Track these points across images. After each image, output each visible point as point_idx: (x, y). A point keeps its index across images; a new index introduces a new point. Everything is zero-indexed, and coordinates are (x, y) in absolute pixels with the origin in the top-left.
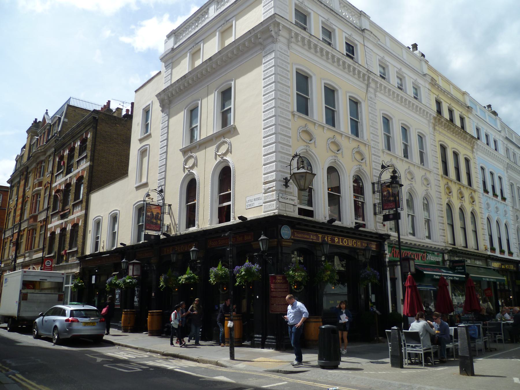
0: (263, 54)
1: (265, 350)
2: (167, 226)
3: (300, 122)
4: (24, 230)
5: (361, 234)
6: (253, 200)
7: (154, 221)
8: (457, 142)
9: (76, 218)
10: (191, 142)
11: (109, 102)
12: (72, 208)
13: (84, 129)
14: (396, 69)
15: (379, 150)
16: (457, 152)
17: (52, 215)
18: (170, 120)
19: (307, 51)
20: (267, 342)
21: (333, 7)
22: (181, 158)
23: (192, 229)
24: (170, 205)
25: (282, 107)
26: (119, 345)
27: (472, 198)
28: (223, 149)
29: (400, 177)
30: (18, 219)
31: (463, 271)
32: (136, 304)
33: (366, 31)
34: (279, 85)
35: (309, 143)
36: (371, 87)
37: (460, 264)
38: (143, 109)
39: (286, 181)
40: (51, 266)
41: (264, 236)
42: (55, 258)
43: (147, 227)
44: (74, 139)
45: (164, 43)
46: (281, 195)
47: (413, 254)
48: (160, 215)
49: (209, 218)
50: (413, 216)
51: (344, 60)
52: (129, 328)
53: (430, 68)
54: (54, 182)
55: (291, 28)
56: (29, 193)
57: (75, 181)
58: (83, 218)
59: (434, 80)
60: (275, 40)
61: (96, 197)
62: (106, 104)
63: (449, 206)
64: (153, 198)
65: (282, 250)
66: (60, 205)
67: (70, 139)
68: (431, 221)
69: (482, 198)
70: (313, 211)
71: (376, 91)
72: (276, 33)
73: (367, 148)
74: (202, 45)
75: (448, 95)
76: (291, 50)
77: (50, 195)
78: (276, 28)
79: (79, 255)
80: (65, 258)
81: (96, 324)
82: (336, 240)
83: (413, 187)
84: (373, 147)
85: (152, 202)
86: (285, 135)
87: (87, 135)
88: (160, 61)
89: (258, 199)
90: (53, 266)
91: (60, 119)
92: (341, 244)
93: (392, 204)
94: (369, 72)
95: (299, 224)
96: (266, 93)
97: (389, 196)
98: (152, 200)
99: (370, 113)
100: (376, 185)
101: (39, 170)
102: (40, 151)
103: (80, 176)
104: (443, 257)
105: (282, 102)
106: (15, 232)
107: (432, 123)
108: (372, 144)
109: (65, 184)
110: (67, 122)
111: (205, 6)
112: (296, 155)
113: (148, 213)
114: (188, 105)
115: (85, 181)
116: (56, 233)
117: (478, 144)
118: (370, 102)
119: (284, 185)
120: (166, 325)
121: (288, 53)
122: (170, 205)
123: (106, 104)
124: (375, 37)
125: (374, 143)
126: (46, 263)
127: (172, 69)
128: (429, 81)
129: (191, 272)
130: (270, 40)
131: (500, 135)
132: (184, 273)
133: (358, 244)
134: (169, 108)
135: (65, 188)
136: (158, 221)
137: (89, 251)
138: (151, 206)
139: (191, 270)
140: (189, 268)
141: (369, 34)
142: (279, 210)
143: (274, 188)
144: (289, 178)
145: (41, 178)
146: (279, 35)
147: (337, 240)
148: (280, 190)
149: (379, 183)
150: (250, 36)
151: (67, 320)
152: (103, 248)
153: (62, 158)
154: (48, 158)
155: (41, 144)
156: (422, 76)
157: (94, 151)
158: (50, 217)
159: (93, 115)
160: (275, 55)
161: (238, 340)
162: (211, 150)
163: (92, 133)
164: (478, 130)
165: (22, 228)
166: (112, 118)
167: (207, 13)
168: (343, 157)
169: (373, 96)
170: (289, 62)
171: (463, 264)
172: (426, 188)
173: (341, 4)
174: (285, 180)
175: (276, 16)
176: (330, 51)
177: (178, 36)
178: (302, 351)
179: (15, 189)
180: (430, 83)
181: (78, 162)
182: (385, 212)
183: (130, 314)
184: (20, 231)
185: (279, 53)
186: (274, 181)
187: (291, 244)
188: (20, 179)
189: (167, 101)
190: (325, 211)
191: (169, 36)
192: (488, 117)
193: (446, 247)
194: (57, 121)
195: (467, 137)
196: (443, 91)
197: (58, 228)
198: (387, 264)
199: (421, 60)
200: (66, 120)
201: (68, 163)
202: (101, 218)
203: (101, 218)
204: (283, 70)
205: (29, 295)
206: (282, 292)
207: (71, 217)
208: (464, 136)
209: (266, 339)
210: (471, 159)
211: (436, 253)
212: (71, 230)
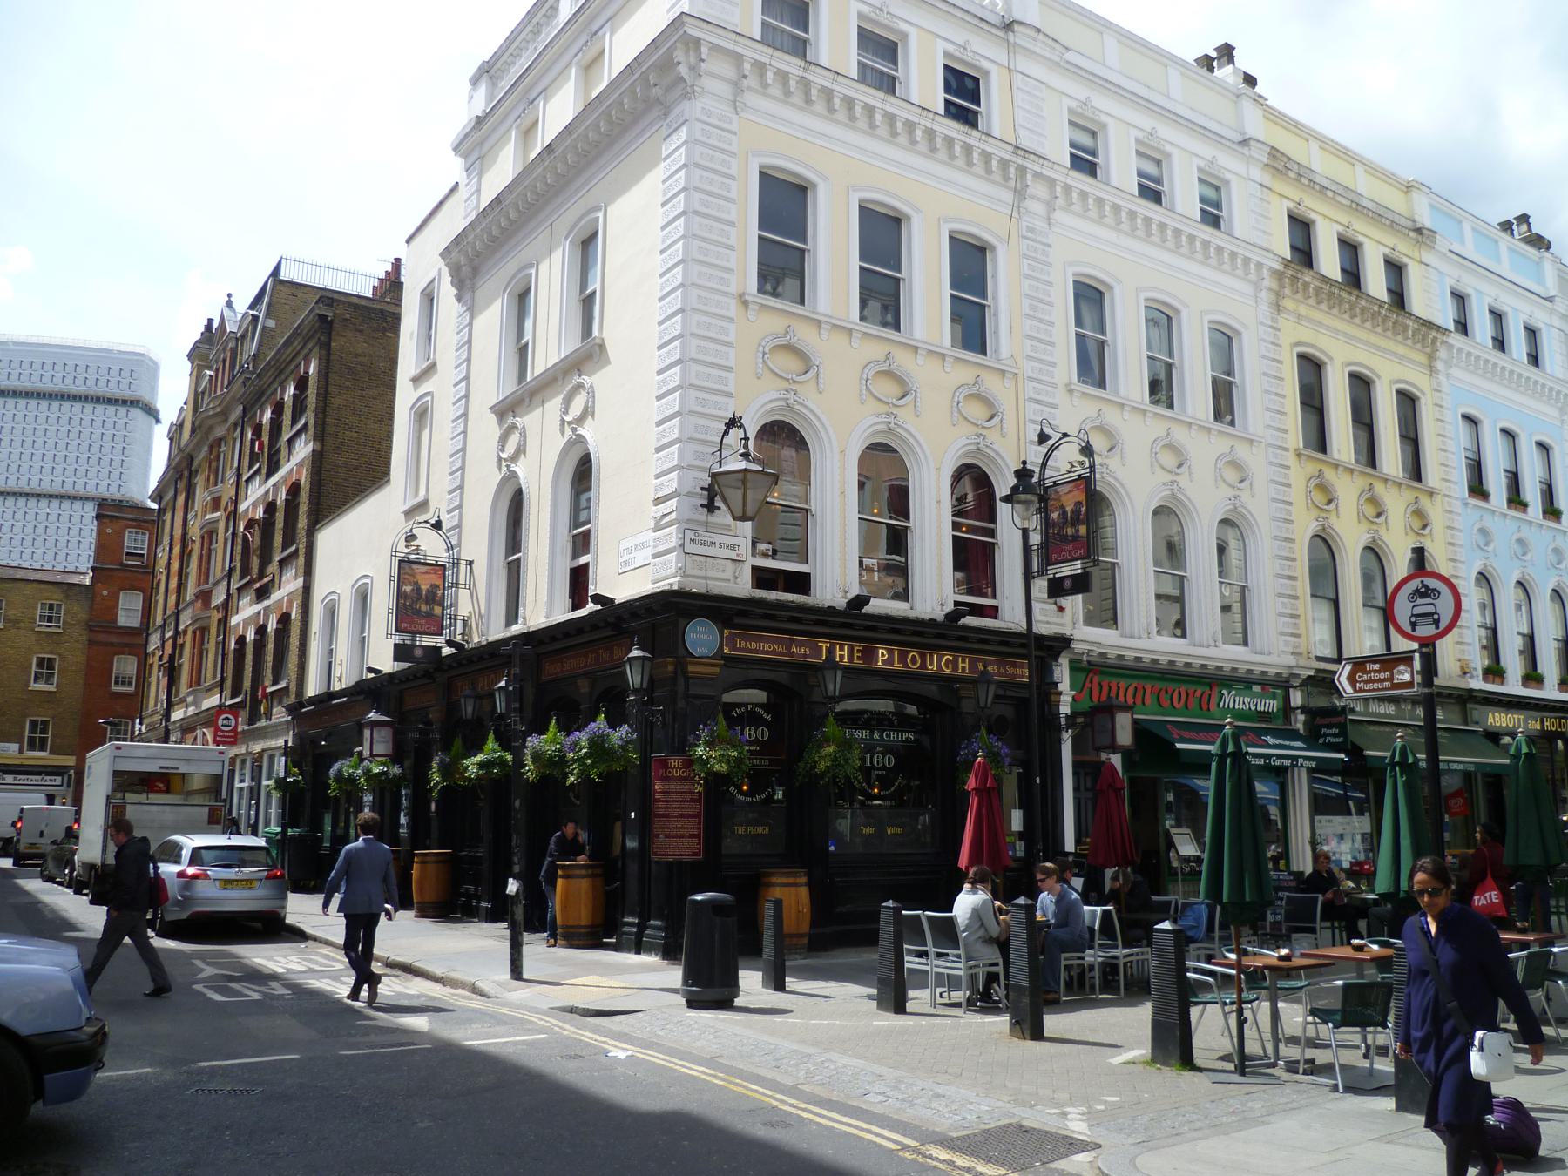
0: (664, 132)
1: (644, 959)
3: (771, 318)
4: (185, 631)
7: (424, 607)
8: (1366, 343)
10: (520, 383)
13: (302, 348)
15: (1054, 385)
16: (1360, 373)
17: (238, 589)
18: (475, 322)
23: (517, 629)
24: (471, 563)
26: (315, 939)
27: (1419, 513)
30: (172, 599)
31: (1341, 740)
33: (1016, 27)
36: (1033, 197)
37: (1334, 720)
38: (422, 293)
40: (235, 730)
42: (245, 707)
43: (404, 625)
44: (283, 377)
46: (690, 534)
47: (1167, 692)
48: (440, 592)
51: (929, 125)
53: (1277, 118)
54: (243, 498)
55: (739, 50)
56: (195, 532)
58: (300, 598)
59: (1279, 155)
65: (687, 688)
66: (255, 562)
67: (275, 379)
68: (1249, 590)
69: (1459, 515)
70: (809, 574)
71: (1051, 207)
72: (692, 68)
73: (1010, 383)
75: (1339, 198)
76: (742, 114)
77: (234, 534)
78: (691, 53)
79: (292, 699)
83: (1181, 490)
84: (1031, 379)
87: (307, 367)
89: (643, 545)
90: (239, 729)
92: (897, 666)
96: (666, 244)
99: (1027, 276)
101: (214, 464)
102: (211, 413)
104: (1287, 699)
105: (704, 269)
106: (167, 636)
107: (1270, 289)
108: (1028, 368)
113: (404, 587)
114: (511, 279)
116: (248, 640)
117: (1451, 346)
119: (702, 505)
120: (463, 890)
121: (731, 123)
122: (471, 563)
123: (390, 269)
124: (1050, 42)
125: (1036, 365)
126: (220, 722)
127: (480, 175)
128: (1262, 162)
129: (497, 746)
130: (678, 92)
131: (1552, 311)
132: (477, 747)
133: (961, 665)
137: (313, 689)
138: (415, 566)
140: (491, 736)
141: (1029, 37)
142: (684, 575)
143: (674, 516)
145: (220, 485)
146: (700, 75)
147: (883, 655)
150: (632, 80)
151: (181, 875)
154: (232, 430)
155: (219, 392)
157: (324, 412)
158: (236, 596)
159: (318, 311)
161: (589, 930)
162: (554, 404)
163: (317, 361)
164: (1460, 299)
165: (181, 628)
169: (1040, 224)
171: (1341, 719)
172: (1231, 492)
174: (706, 493)
175: (685, 19)
179: (168, 516)
180: (1267, 165)
181: (291, 441)
182: (1054, 571)
184: (177, 633)
187: (717, 670)
188: (176, 488)
190: (846, 575)
191: (475, 81)
192: (1509, 255)
193: (1290, 667)
195: (1406, 328)
196: (1317, 187)
199: (1238, 96)
200: (271, 323)
202: (336, 598)
205: (129, 808)
208: (1394, 323)
209: (646, 929)
210: (1424, 394)
211: (1257, 689)
212: (277, 629)
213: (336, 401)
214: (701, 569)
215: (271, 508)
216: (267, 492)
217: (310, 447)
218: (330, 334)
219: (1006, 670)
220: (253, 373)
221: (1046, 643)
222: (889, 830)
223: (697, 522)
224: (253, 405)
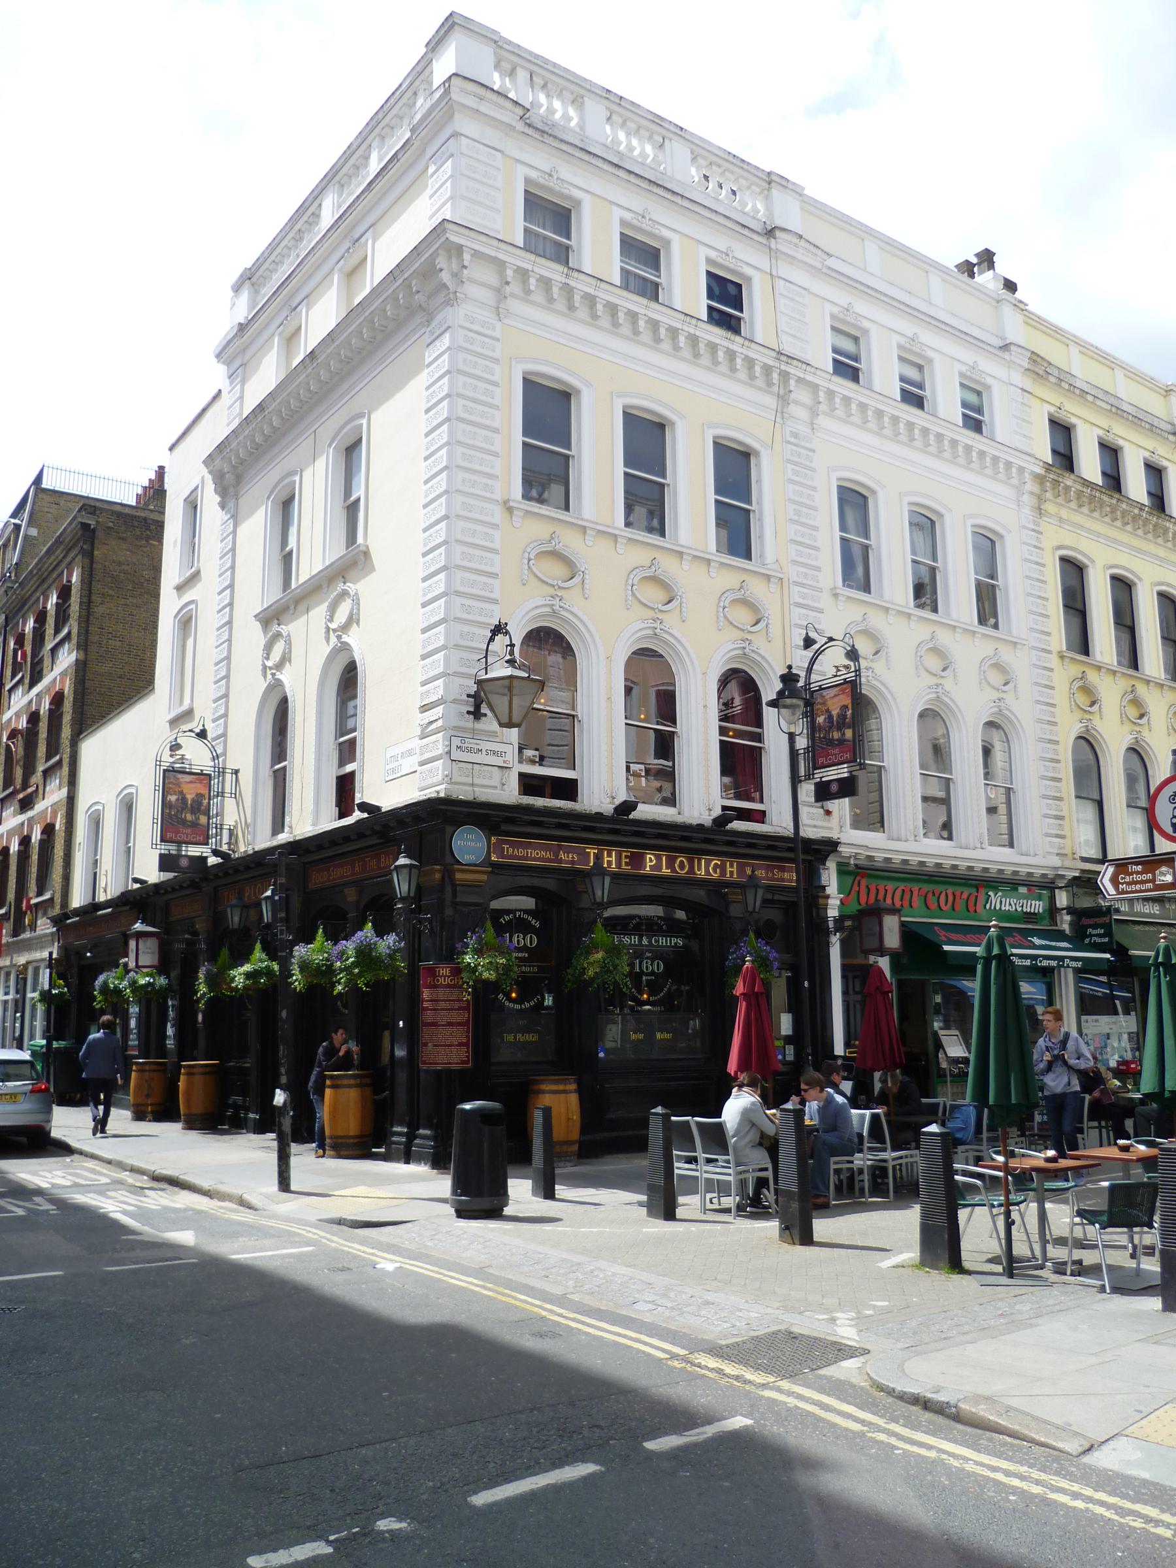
2: (230, 829)
5: (734, 841)
7: (189, 817)
13: (65, 557)
14: (896, 339)
15: (820, 590)
19: (566, 315)
20: (418, 1146)
21: (669, 173)
23: (283, 838)
24: (236, 772)
25: (471, 490)
31: (1106, 940)
32: (170, 1043)
34: (461, 426)
35: (560, 588)
36: (796, 403)
38: (185, 500)
41: (404, 857)
42: (9, 919)
44: (45, 586)
46: (456, 742)
48: (205, 802)
49: (312, 807)
50: (949, 779)
51: (692, 331)
52: (150, 1108)
55: (501, 256)
59: (1039, 360)
60: (451, 296)
61: (93, 748)
62: (153, 477)
63: (1087, 743)
71: (814, 413)
72: (455, 275)
74: (304, 311)
75: (1099, 403)
76: (506, 321)
79: (57, 911)
80: (29, 920)
81: (21, 1098)
83: (947, 693)
84: (797, 583)
86: (476, 570)
87: (70, 575)
88: (216, 360)
89: (410, 753)
92: (666, 871)
94: (784, 358)
95: (511, 821)
104: (1052, 899)
107: (1032, 493)
108: (793, 573)
110: (34, 538)
111: (311, 199)
118: (790, 447)
119: (468, 712)
120: (230, 1102)
122: (236, 772)
123: (153, 477)
124: (812, 248)
127: (243, 382)
128: (1021, 366)
129: (264, 956)
130: (440, 298)
133: (729, 869)
135: (30, 726)
136: (201, 817)
138: (180, 776)
139: (264, 949)
140: (258, 946)
143: (440, 723)
147: (651, 860)
148: (455, 728)
150: (395, 286)
152: (105, 891)
153: (20, 640)
156: (996, 351)
157: (87, 621)
159: (80, 520)
160: (452, 339)
161: (358, 1140)
162: (319, 612)
163: (80, 570)
166: (136, 524)
167: (316, 216)
169: (803, 429)
170: (497, 355)
171: (1107, 920)
174: (472, 700)
175: (447, 225)
176: (641, 310)
177: (259, 286)
178: (510, 1171)
181: (54, 650)
182: (821, 775)
183: (150, 1071)
185: (462, 332)
186: (441, 701)
187: (484, 877)
189: (229, 478)
191: (237, 288)
193: (1056, 868)
195: (1166, 530)
196: (1077, 392)
197: (14, 836)
199: (998, 302)
200: (33, 532)
201: (33, 658)
203: (101, 808)
204: (475, 382)
206: (449, 1010)
207: (40, 806)
213: (99, 610)
215: (34, 718)
216: (31, 702)
219: (774, 874)
222: (659, 1036)
223: (463, 729)
224: (16, 613)
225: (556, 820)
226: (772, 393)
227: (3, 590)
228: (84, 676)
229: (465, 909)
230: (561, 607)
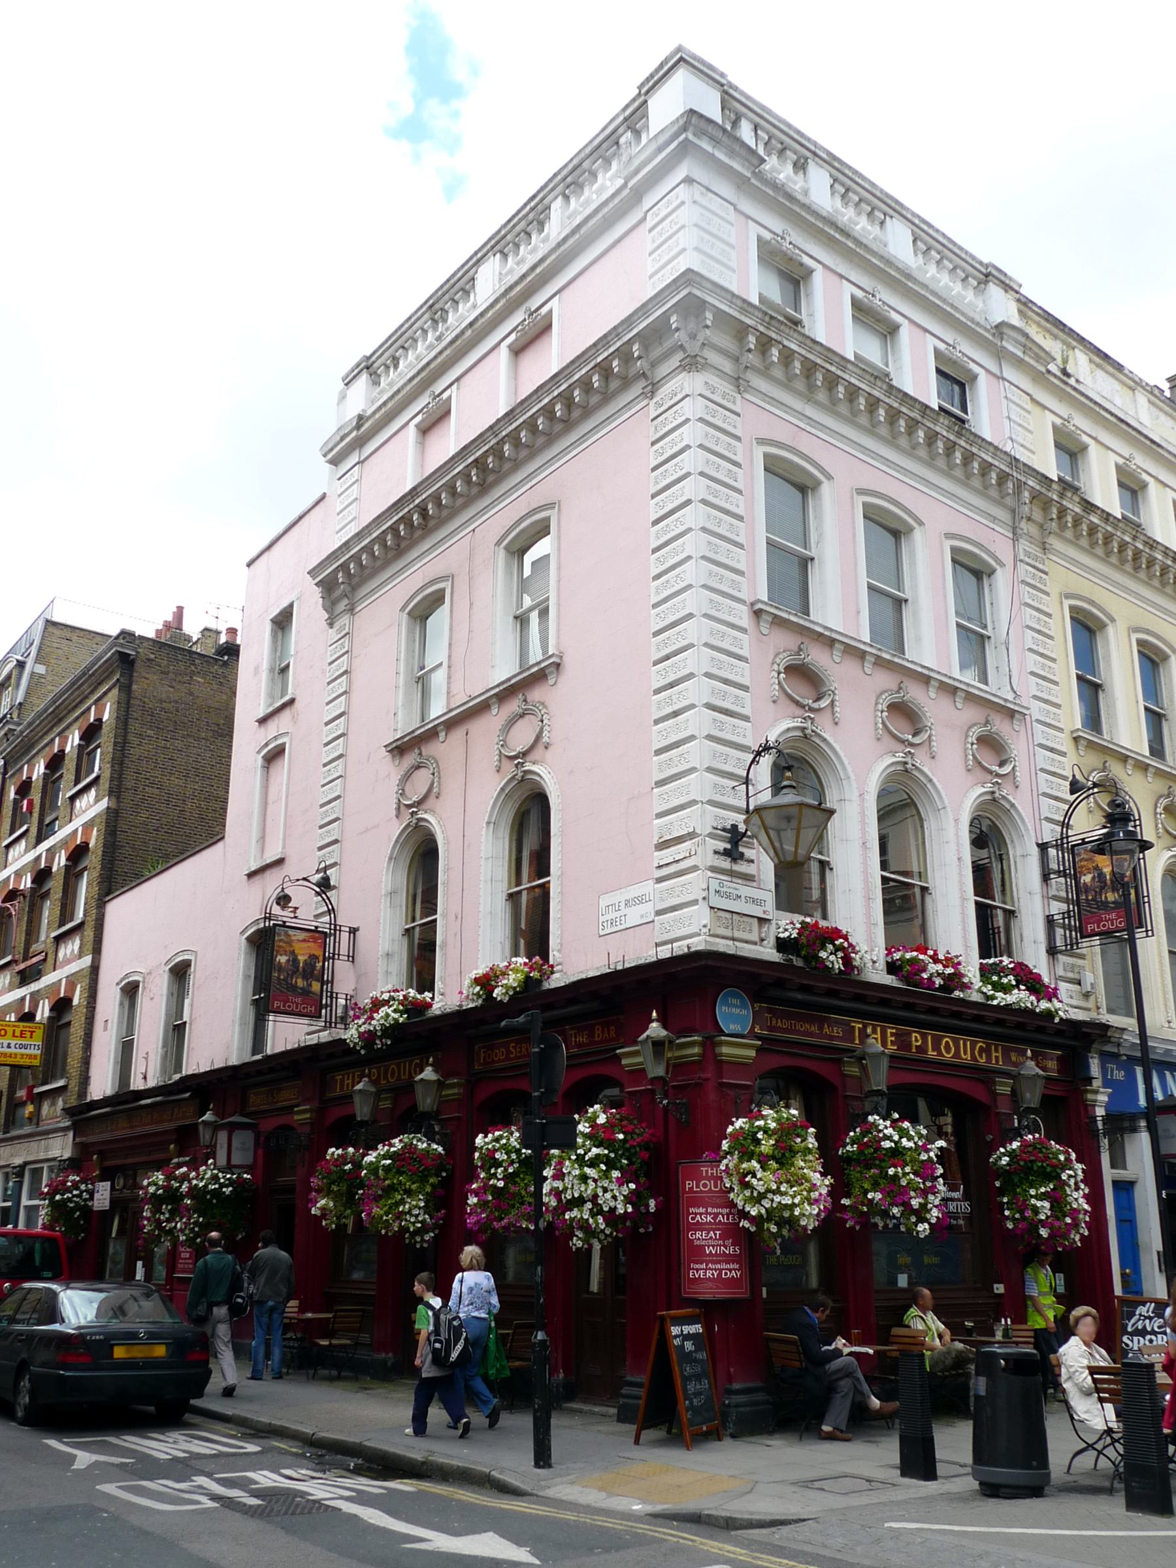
6: (622, 904)
7: (300, 983)
9: (64, 980)
11: (180, 609)
12: (53, 949)
22: (389, 771)
24: (353, 931)
28: (522, 736)
29: (1140, 819)
35: (811, 710)
39: (735, 837)
45: (336, 401)
57: (63, 862)
61: (120, 910)
64: (296, 908)
79: (73, 1101)
82: (916, 1039)
85: (294, 920)
89: (640, 900)
91: (21, 665)
92: (931, 1053)
93: (1113, 916)
97: (1102, 888)
98: (294, 912)
100: (1052, 852)
103: (78, 846)
109: (35, 873)
110: (41, 676)
112: (766, 748)
115: (93, 860)
121: (734, 403)
122: (353, 931)
133: (994, 1054)
134: (351, 610)
136: (314, 983)
137: (102, 1085)
138: (291, 932)
144: (742, 828)
147: (917, 1040)
149: (1062, 844)
152: (145, 1078)
166: (180, 657)
168: (933, 758)
173: (919, 243)
194: (11, 671)
198: (1100, 1127)
200: (41, 669)
213: (135, 752)
214: (727, 928)
215: (42, 876)
216: (38, 858)
217: (104, 804)
218: (131, 676)
220: (19, 724)
221: (1084, 1030)
224: (19, 758)
225: (827, 985)
226: (1005, 506)
227: (3, 732)
228: (115, 826)
229: (731, 1093)
230: (813, 731)
